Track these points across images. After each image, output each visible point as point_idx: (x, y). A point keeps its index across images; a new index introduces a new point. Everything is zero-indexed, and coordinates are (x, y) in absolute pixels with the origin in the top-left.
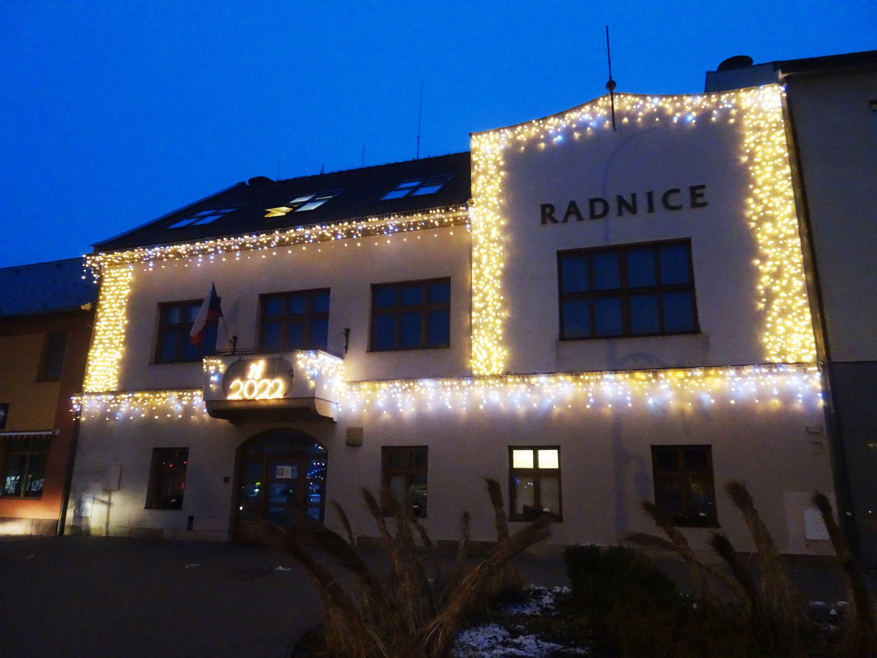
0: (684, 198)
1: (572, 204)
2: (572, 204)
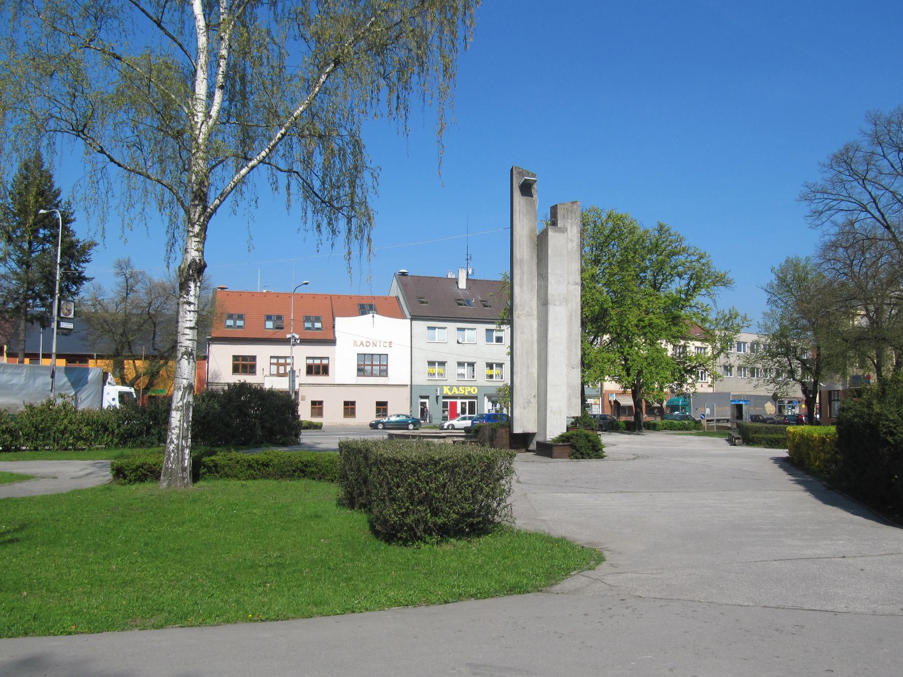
0: (387, 344)
1: (362, 342)
2: (362, 342)
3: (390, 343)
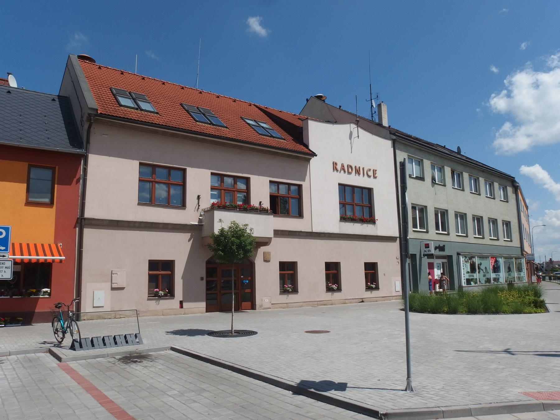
0: (371, 173)
3: (375, 171)
